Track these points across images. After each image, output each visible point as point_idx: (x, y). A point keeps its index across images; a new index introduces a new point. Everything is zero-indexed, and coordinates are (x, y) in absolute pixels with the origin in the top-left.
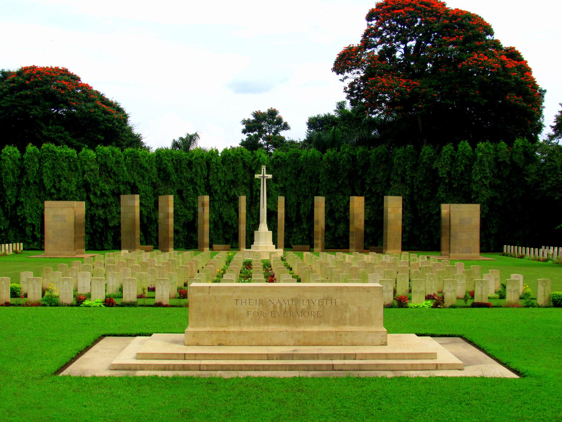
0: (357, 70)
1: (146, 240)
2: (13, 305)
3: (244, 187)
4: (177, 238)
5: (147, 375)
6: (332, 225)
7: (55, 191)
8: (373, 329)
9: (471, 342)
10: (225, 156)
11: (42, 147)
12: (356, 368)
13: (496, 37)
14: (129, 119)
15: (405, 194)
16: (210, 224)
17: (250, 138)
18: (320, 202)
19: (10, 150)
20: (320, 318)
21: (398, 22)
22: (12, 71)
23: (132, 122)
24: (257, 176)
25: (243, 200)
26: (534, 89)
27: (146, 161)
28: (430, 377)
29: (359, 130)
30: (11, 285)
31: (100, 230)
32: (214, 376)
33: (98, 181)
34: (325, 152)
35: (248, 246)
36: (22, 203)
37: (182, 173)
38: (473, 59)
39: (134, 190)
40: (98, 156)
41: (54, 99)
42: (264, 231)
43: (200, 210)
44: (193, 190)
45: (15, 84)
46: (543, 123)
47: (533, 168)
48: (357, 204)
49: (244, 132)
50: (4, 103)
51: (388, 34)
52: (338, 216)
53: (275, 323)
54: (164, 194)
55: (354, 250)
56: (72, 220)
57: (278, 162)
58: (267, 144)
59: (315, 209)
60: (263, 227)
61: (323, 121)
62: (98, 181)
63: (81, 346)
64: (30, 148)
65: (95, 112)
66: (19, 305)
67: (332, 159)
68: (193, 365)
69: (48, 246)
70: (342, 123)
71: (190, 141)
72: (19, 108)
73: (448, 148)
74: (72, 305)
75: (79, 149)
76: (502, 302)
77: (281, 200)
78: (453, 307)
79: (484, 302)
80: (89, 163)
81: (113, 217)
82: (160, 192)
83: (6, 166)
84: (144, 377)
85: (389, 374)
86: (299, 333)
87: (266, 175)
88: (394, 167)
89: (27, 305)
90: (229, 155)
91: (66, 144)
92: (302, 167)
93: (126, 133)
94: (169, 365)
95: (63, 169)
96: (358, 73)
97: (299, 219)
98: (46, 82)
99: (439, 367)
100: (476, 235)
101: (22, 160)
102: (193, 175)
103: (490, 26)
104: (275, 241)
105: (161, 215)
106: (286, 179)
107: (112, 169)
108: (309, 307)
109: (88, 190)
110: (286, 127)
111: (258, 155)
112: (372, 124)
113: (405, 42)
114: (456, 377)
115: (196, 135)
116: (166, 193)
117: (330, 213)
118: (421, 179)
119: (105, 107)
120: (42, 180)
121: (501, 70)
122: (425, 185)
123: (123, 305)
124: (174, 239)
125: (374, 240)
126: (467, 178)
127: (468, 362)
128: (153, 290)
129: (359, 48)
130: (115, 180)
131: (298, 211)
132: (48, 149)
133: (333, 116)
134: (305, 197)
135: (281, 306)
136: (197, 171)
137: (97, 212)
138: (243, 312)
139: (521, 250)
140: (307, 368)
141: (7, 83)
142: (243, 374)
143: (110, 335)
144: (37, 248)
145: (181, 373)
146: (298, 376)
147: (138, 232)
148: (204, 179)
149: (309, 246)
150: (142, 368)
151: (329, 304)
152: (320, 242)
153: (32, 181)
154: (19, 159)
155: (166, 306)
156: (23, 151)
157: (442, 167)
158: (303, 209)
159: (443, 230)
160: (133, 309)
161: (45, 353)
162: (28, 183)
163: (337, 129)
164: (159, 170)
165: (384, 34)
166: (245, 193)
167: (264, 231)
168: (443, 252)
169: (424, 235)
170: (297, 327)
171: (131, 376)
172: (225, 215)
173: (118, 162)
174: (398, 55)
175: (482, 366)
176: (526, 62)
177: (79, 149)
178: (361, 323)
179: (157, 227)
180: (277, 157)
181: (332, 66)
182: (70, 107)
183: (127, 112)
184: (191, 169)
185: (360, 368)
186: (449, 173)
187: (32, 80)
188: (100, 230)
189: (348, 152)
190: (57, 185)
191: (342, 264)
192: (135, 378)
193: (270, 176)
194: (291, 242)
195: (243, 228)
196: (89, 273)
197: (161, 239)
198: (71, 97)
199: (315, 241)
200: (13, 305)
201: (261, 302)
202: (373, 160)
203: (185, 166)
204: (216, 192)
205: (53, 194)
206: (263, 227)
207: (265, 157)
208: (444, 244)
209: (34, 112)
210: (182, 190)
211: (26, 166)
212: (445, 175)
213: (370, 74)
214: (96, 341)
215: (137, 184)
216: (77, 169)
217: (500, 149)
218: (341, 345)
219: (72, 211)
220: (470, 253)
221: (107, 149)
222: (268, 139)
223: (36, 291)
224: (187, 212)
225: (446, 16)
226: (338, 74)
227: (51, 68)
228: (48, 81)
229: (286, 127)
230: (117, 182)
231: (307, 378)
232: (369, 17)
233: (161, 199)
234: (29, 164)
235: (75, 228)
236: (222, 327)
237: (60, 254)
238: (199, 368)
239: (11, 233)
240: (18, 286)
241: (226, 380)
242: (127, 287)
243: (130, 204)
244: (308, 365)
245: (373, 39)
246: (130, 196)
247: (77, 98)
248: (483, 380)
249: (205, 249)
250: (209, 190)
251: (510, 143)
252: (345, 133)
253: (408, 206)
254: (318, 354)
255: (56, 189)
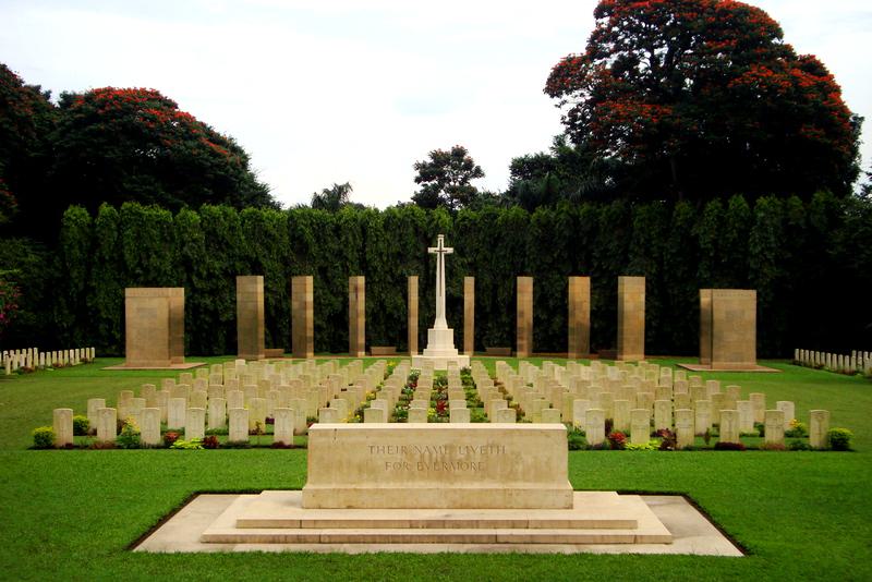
0: (580, 92)
1: (274, 340)
2: (77, 447)
3: (416, 264)
4: (318, 337)
5: (248, 551)
6: (544, 317)
7: (141, 272)
8: (554, 486)
9: (694, 504)
10: (389, 218)
11: (123, 208)
12: (528, 540)
13: (786, 40)
14: (250, 162)
15: (650, 273)
16: (366, 317)
17: (426, 191)
18: (525, 285)
19: (76, 213)
20: (483, 472)
21: (642, 19)
22: (77, 93)
23: (254, 166)
24: (431, 250)
25: (414, 282)
26: (843, 117)
27: (274, 226)
28: (621, 555)
29: (586, 177)
30: (73, 418)
31: (206, 327)
32: (336, 551)
33: (203, 256)
34: (534, 211)
35: (420, 352)
36: (93, 288)
37: (325, 242)
38: (756, 74)
39: (256, 269)
40: (203, 219)
41: (140, 136)
42: (441, 330)
43: (352, 296)
44: (342, 266)
45: (82, 115)
46: (860, 167)
47: (839, 236)
48: (580, 289)
49: (418, 180)
50: (67, 143)
51: (626, 37)
52: (552, 305)
53: (422, 478)
54: (300, 274)
55: (575, 355)
56: (165, 315)
57: (465, 225)
58: (452, 198)
59: (519, 295)
60: (441, 323)
61: (533, 164)
62: (203, 256)
63: (165, 509)
64: (105, 208)
65: (199, 154)
66: (86, 447)
67: (543, 221)
68: (310, 536)
69: (131, 352)
70: (561, 166)
71: (339, 194)
72: (88, 150)
73: (713, 205)
74: (158, 447)
75: (175, 209)
76: (758, 442)
77: (469, 282)
78: (688, 449)
79: (733, 442)
80: (190, 230)
81: (226, 309)
82: (294, 271)
83: (71, 235)
84: (243, 553)
85: (568, 550)
86: (455, 491)
87: (443, 249)
88: (634, 235)
89: (96, 447)
90: (394, 217)
91: (157, 202)
92: (500, 233)
93: (245, 183)
94: (279, 536)
95: (152, 239)
96: (582, 95)
97: (495, 306)
98: (128, 111)
99: (639, 541)
100: (751, 335)
101: (92, 226)
102: (342, 246)
103: (777, 25)
104: (459, 344)
105: (295, 305)
106: (477, 251)
107: (223, 238)
108: (468, 457)
109: (189, 270)
110: (478, 173)
111: (436, 216)
112: (604, 169)
113: (651, 50)
114: (657, 555)
115: (348, 185)
116: (303, 273)
117: (540, 301)
118: (674, 251)
119: (213, 146)
120: (122, 255)
121: (793, 89)
122: (679, 259)
123: (229, 446)
124: (315, 339)
125: (604, 341)
126: (742, 250)
127: (696, 532)
128: (270, 421)
129: (584, 59)
130: (228, 254)
131: (495, 297)
132: (130, 209)
133: (549, 156)
134: (505, 277)
135: (431, 454)
136: (347, 238)
137: (203, 301)
138: (381, 463)
139: (818, 357)
140: (462, 540)
141: (70, 113)
142: (374, 549)
143: (206, 492)
144: (116, 354)
145: (294, 548)
146: (446, 552)
147: (262, 330)
148: (358, 251)
149: (509, 349)
150: (243, 539)
151: (495, 453)
152: (525, 342)
153: (107, 258)
154: (88, 225)
155: (289, 447)
156: (94, 213)
157: (705, 233)
158: (502, 295)
159: (704, 328)
160: (244, 451)
161: (116, 519)
162: (102, 259)
163: (553, 177)
164: (293, 239)
165: (620, 38)
166: (417, 272)
167: (441, 330)
168: (703, 360)
169: (678, 335)
170: (452, 483)
171: (227, 551)
172: (387, 303)
173: (232, 228)
174: (642, 66)
175: (699, 539)
176: (832, 77)
177: (175, 209)
178: (538, 478)
179: (290, 322)
180: (464, 219)
181: (545, 86)
182: (163, 147)
183: (246, 152)
184: (339, 237)
185: (532, 540)
186: (714, 242)
187: (107, 108)
188: (206, 327)
189: (567, 212)
190: (145, 263)
191: (547, 382)
192: (232, 554)
193: (450, 250)
194: (484, 343)
195: (414, 323)
196: (183, 400)
197: (295, 339)
198: (163, 132)
199: (519, 342)
200: (77, 447)
201: (404, 450)
202: (603, 223)
203: (332, 232)
204: (375, 270)
205: (139, 275)
206: (441, 323)
207: (446, 218)
208: (704, 348)
209: (110, 155)
210: (327, 268)
211: (99, 235)
212: (710, 245)
213: (598, 97)
214: (186, 501)
215: (261, 259)
216: (173, 239)
217: (792, 206)
218: (512, 508)
219: (165, 302)
220: (742, 361)
221: (216, 209)
222: (452, 190)
223: (109, 428)
224: (333, 299)
225: (712, 11)
226: (552, 96)
227: (135, 90)
228: (129, 109)
229: (478, 173)
230: (231, 257)
231: (458, 555)
232: (599, 13)
233: (295, 281)
234: (103, 232)
235: (170, 326)
236: (352, 483)
237: (148, 365)
238: (319, 540)
239: (78, 333)
240: (83, 418)
241: (352, 557)
242: (235, 421)
243: (251, 290)
244: (463, 536)
245: (605, 45)
246: (250, 278)
247: (173, 134)
248: (693, 560)
249: (359, 353)
250: (365, 268)
251: (806, 199)
252: (565, 183)
253: (656, 291)
254: (477, 521)
255: (142, 269)
